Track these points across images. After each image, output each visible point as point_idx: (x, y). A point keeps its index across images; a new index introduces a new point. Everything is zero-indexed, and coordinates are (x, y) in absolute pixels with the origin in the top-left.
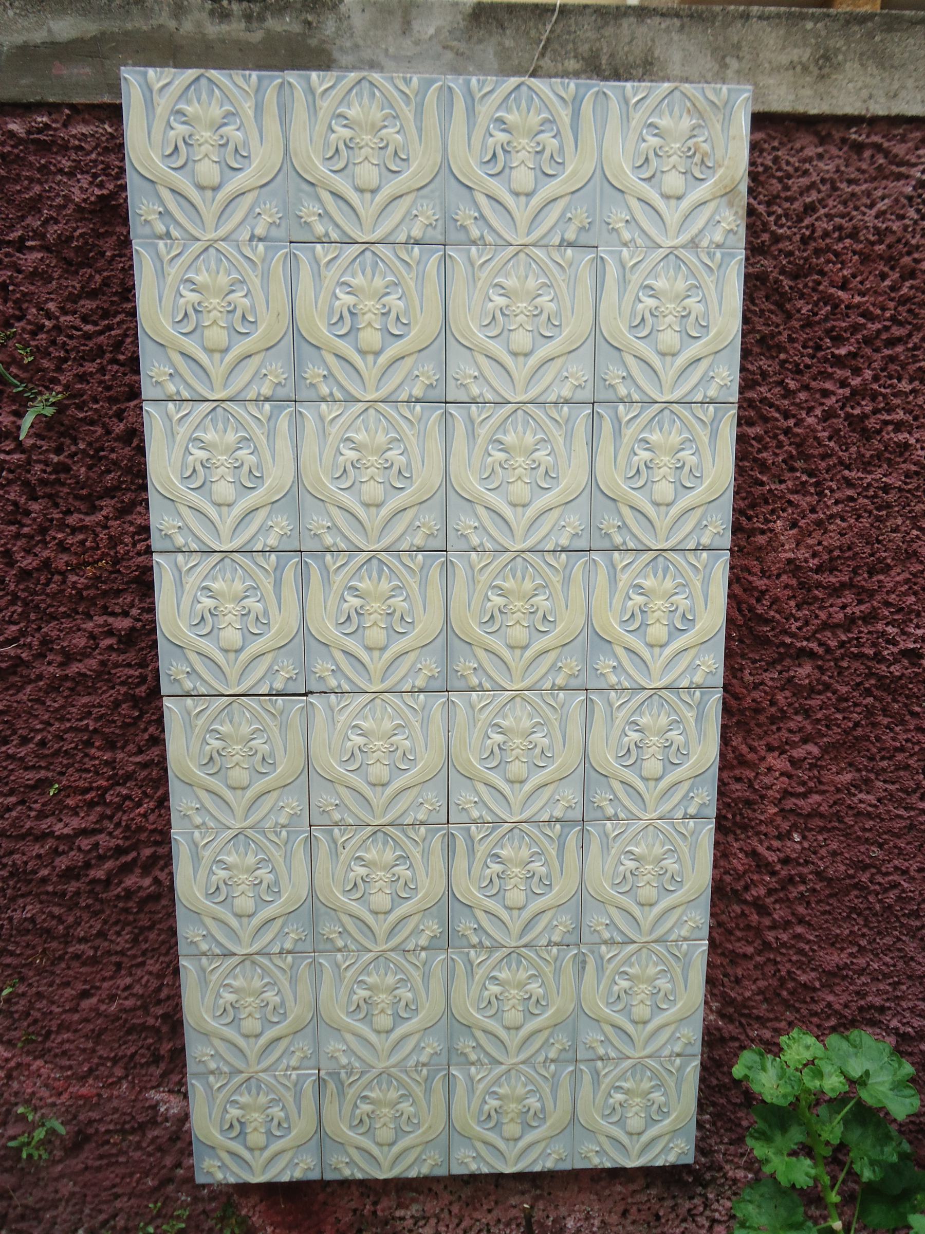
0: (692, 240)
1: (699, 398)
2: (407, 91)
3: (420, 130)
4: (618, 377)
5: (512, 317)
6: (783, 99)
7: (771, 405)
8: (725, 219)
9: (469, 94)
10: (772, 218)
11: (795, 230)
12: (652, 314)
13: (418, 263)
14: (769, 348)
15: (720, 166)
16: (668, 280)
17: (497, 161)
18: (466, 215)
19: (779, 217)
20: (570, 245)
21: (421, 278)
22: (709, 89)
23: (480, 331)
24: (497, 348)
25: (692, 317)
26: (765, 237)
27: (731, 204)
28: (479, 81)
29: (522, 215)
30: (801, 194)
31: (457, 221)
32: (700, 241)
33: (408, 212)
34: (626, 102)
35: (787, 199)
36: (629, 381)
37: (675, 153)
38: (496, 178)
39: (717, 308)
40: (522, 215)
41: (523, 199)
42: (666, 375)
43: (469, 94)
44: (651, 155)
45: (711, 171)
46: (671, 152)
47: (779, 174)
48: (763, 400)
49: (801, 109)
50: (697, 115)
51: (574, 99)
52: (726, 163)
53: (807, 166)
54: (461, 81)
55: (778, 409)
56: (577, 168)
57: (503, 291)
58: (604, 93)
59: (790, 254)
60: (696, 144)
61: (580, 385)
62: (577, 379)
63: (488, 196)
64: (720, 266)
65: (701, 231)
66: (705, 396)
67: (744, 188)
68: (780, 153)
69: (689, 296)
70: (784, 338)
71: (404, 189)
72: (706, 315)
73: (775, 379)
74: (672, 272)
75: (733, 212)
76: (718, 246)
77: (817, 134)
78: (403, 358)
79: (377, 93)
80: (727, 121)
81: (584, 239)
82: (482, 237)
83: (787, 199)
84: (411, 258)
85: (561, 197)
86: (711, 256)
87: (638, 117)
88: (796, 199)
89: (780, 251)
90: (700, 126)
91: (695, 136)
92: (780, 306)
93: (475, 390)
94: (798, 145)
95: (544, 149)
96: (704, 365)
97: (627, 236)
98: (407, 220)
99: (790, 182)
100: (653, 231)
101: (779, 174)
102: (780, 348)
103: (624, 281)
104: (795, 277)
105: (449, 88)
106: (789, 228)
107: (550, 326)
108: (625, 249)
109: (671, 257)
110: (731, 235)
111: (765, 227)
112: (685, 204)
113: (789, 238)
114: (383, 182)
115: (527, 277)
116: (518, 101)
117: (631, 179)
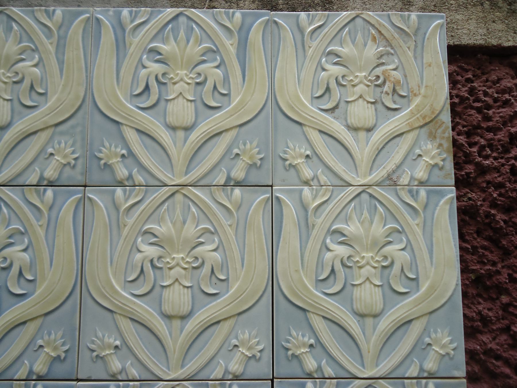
0: (389, 177)
1: (413, 371)
2: (49, 24)
3: (61, 63)
4: (304, 345)
5: (166, 270)
6: (475, 32)
7: (498, 357)
8: (427, 152)
9: (120, 26)
10: (475, 149)
11: (502, 161)
12: (344, 265)
13: (51, 208)
14: (487, 289)
15: (415, 95)
16: (362, 223)
17: (150, 94)
18: (110, 151)
19: (482, 148)
20: (238, 184)
21: (51, 226)
22: (396, 17)
23: (124, 289)
24: (144, 309)
25: (396, 268)
26: (470, 168)
27: (432, 136)
28: (131, 12)
29: (179, 152)
30: (505, 124)
31: (100, 159)
32: (398, 178)
33: (43, 150)
34: (301, 31)
35: (489, 129)
36: (318, 350)
37: (361, 82)
38: (149, 112)
39: (426, 256)
40: (179, 152)
41: (181, 134)
42: (368, 342)
43: (120, 26)
44: (333, 85)
45: (405, 100)
46: (356, 81)
47: (478, 105)
48: (488, 352)
49: (494, 42)
50: (384, 42)
51: (240, 29)
52: (423, 91)
53: (507, 96)
54: (111, 13)
55: (507, 362)
56: (246, 98)
57: (154, 240)
58: (276, 22)
59: (499, 186)
60: (384, 72)
61: (254, 356)
62: (250, 349)
63: (138, 130)
64: (426, 207)
65: (398, 167)
66: (422, 370)
67: (446, 118)
68: (475, 84)
69: (390, 243)
70: (503, 278)
71: (39, 125)
72: (414, 264)
73: (499, 326)
74: (366, 214)
75: (436, 144)
76: (422, 183)
77: (511, 66)
78: (24, 323)
79: (15, 27)
80: (419, 50)
81: (255, 178)
82: (130, 177)
83: (489, 129)
84: (42, 202)
85: (227, 130)
86: (414, 195)
87: (315, 46)
88: (500, 129)
89: (488, 182)
90: (388, 54)
91: (383, 64)
92: (495, 242)
93: (116, 365)
94: (494, 77)
95: (206, 79)
96: (416, 328)
97: (307, 173)
98: (41, 159)
99: (490, 112)
100: (340, 168)
101: (478, 105)
102: (500, 290)
103: (306, 227)
104: (507, 210)
105: (98, 20)
106: (495, 159)
107: (214, 280)
108: (306, 188)
109: (364, 196)
110: (436, 171)
111: (468, 159)
112: (377, 136)
113: (497, 170)
114: (378, 124)
115: (184, 222)
116: (175, 32)
117: (311, 111)
